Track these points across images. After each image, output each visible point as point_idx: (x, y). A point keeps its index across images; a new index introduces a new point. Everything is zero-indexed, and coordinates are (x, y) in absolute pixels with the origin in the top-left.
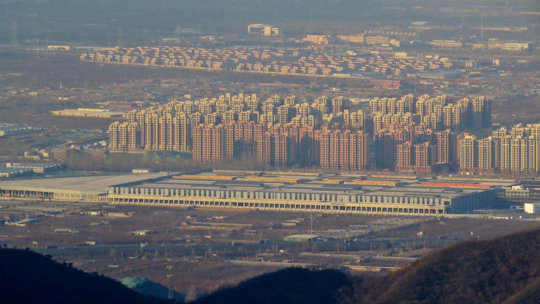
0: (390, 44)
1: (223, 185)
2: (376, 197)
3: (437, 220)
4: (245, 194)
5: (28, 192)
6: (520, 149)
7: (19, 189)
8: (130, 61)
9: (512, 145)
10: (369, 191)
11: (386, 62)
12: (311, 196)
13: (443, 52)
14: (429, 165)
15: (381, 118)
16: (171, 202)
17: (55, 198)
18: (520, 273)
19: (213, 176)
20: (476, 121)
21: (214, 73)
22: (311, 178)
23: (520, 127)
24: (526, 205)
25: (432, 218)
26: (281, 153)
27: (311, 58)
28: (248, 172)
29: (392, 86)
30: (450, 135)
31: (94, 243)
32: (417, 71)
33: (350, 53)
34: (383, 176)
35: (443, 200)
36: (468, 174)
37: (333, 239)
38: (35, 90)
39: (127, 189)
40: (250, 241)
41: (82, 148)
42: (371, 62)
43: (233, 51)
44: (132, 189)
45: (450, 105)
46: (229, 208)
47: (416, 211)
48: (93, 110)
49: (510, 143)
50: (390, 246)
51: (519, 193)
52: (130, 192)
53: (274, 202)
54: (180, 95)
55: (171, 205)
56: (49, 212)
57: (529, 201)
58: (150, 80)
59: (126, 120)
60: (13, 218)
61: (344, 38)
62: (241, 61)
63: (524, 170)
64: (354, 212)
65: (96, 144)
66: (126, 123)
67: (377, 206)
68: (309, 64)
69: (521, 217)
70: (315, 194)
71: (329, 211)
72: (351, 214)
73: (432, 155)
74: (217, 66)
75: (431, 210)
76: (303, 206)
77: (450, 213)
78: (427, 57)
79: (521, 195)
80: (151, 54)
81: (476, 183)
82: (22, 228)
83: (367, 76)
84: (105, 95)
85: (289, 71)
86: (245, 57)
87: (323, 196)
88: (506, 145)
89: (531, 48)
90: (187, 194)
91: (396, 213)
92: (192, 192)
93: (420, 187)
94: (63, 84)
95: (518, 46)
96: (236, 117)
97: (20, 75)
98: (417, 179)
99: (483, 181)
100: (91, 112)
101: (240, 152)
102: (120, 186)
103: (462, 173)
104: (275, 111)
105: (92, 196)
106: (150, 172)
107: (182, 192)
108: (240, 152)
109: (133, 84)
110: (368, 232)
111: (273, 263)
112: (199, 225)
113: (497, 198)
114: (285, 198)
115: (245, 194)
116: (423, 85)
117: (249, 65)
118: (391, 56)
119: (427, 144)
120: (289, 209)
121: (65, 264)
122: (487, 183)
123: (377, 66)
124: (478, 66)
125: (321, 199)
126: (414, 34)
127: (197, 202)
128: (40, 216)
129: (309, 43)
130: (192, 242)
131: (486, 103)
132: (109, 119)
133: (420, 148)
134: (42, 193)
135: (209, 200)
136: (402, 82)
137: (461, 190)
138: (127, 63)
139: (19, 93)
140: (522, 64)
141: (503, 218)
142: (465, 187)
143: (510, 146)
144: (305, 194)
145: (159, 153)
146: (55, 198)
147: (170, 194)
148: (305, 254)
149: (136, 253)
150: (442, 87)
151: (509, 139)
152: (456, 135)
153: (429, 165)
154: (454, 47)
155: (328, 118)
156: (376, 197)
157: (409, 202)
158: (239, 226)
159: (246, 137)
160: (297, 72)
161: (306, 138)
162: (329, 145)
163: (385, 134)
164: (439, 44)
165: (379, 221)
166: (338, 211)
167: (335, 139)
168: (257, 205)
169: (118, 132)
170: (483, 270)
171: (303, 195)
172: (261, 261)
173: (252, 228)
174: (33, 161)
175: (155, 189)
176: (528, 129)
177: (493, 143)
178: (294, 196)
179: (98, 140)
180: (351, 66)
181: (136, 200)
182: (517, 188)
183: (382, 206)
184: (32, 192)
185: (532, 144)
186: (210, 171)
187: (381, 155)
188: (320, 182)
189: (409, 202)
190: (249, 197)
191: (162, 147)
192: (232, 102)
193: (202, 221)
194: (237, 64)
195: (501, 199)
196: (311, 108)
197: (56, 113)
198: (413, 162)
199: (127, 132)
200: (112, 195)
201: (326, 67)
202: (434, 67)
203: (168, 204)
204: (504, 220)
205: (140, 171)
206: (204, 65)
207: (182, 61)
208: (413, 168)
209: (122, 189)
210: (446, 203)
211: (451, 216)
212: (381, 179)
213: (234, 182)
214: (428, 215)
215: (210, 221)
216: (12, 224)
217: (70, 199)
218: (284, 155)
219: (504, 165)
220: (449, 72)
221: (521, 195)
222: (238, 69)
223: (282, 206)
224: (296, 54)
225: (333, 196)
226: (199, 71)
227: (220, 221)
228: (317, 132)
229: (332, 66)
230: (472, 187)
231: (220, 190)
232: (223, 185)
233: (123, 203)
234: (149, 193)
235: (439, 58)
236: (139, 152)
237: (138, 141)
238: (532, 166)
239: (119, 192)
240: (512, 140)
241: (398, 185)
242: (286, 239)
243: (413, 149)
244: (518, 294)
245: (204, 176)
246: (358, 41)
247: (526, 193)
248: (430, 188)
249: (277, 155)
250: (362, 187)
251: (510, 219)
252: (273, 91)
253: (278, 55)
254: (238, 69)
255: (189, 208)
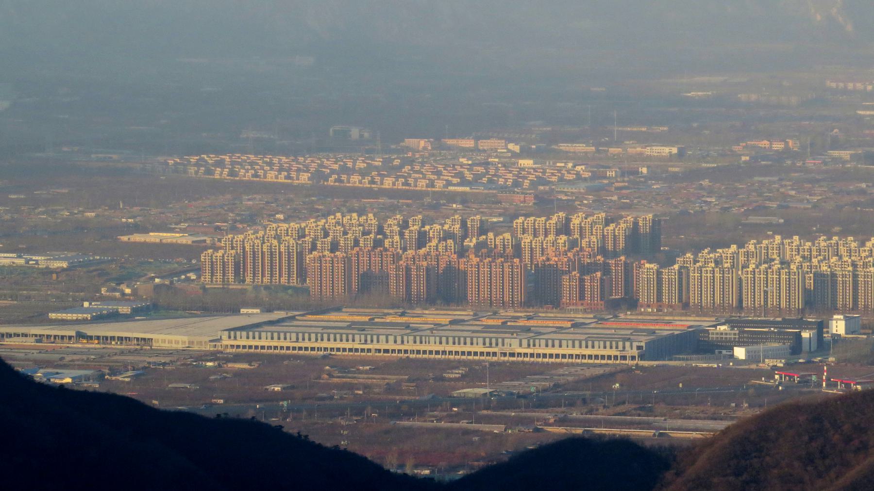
0: (507, 149)
1: (361, 327)
2: (553, 340)
4: (391, 338)
5: (121, 339)
7: (109, 334)
8: (197, 172)
9: (704, 275)
10: (540, 334)
11: (511, 172)
12: (472, 340)
13: (578, 159)
15: (531, 242)
16: (300, 349)
17: (155, 345)
18: (856, 443)
19: (344, 317)
20: (639, 244)
21: (302, 187)
22: (466, 318)
23: (709, 253)
24: (736, 349)
26: (419, 286)
27: (417, 168)
28: (386, 311)
29: (525, 202)
30: (625, 263)
31: (222, 401)
32: (550, 182)
33: (463, 160)
34: (552, 315)
35: (635, 344)
37: (512, 394)
38: (92, 209)
39: (244, 334)
40: (411, 398)
41: (172, 283)
42: (492, 172)
43: (319, 159)
44: (251, 334)
45: (612, 226)
46: (372, 356)
47: (603, 357)
48: (169, 235)
50: (584, 401)
51: (726, 334)
52: (248, 338)
53: (427, 348)
54: (270, 216)
55: (301, 352)
56: (155, 363)
57: (740, 344)
58: (229, 196)
59: (221, 248)
60: (114, 372)
61: (450, 142)
62: (333, 172)
63: (719, 305)
64: (527, 359)
65: (183, 277)
66: (222, 251)
67: (555, 351)
68: (417, 175)
70: (477, 338)
71: (495, 359)
72: (523, 362)
73: (605, 287)
74: (304, 178)
76: (463, 353)
78: (558, 164)
80: (220, 164)
81: (669, 323)
82: (128, 383)
83: (490, 189)
84: (178, 215)
85: (394, 184)
86: (336, 167)
87: (487, 340)
89: (681, 154)
90: (319, 339)
91: (579, 361)
92: (325, 336)
94: (123, 202)
95: (666, 150)
96: (356, 242)
97: (67, 191)
98: (594, 317)
100: (167, 237)
101: (367, 286)
102: (235, 329)
104: (402, 234)
105: (201, 342)
106: (262, 311)
107: (313, 336)
108: (367, 286)
109: (208, 202)
110: (552, 384)
111: (449, 425)
112: (343, 377)
114: (441, 343)
115: (391, 338)
116: (561, 200)
117: (344, 177)
118: (514, 164)
119: (599, 274)
120: (440, 356)
121: (300, 436)
122: (682, 323)
123: (500, 177)
124: (623, 175)
125: (484, 344)
126: (534, 136)
127: (332, 349)
128: (145, 368)
129: (408, 149)
130: (342, 398)
131: (656, 223)
132: (190, 245)
134: (138, 339)
135: (348, 346)
136: (536, 197)
137: (653, 332)
138: (194, 175)
139: (72, 214)
140: (675, 173)
142: (657, 327)
143: (754, 278)
144: (465, 338)
145: (267, 288)
146: (155, 345)
147: (298, 338)
148: (485, 412)
149: (279, 414)
150: (585, 202)
151: (701, 267)
152: (632, 264)
153: (601, 300)
154: (586, 153)
155: (471, 242)
156: (553, 340)
157: (593, 347)
158: (393, 379)
159: (373, 268)
160: (403, 184)
161: (449, 268)
162: (478, 277)
163: (547, 263)
164: (567, 149)
165: (561, 371)
166: (506, 359)
167: (486, 269)
168: (406, 351)
169: (212, 262)
170: (811, 439)
171: (462, 340)
172: (433, 421)
173: (409, 381)
174: (114, 299)
175: (279, 333)
177: (680, 273)
178: (451, 340)
179: (185, 272)
180: (469, 176)
181: (256, 347)
182: (723, 328)
183: (561, 351)
184: (126, 338)
186: (338, 309)
187: (542, 289)
188: (478, 323)
190: (395, 342)
191: (266, 280)
192: (350, 224)
193: (345, 372)
194: (330, 175)
196: (445, 231)
197: (125, 238)
198: (582, 297)
199: (224, 262)
200: (226, 342)
201: (439, 179)
202: (571, 177)
203: (295, 352)
205: (250, 311)
206: (288, 177)
207: (261, 173)
208: (582, 304)
209: (238, 333)
210: (639, 348)
211: (646, 363)
212: (547, 319)
213: (371, 322)
214: (618, 362)
215: (354, 372)
216: (114, 378)
217: (174, 346)
218: (423, 289)
219: (694, 299)
220: (588, 184)
222: (331, 181)
223: (437, 352)
224: (397, 162)
225: (500, 340)
226: (283, 185)
227: (366, 372)
228: (462, 260)
229: (446, 178)
230: (666, 328)
231: (360, 335)
232: (361, 327)
233: (240, 350)
234: (272, 338)
235: (574, 166)
236: (240, 287)
237: (237, 272)
239: (235, 338)
241: (573, 326)
242: (455, 393)
243: (582, 281)
244: (858, 468)
245: (333, 316)
246: (467, 146)
247: (735, 334)
248: (615, 329)
249: (414, 287)
252: (382, 208)
253: (376, 163)
254: (331, 181)
255: (324, 357)
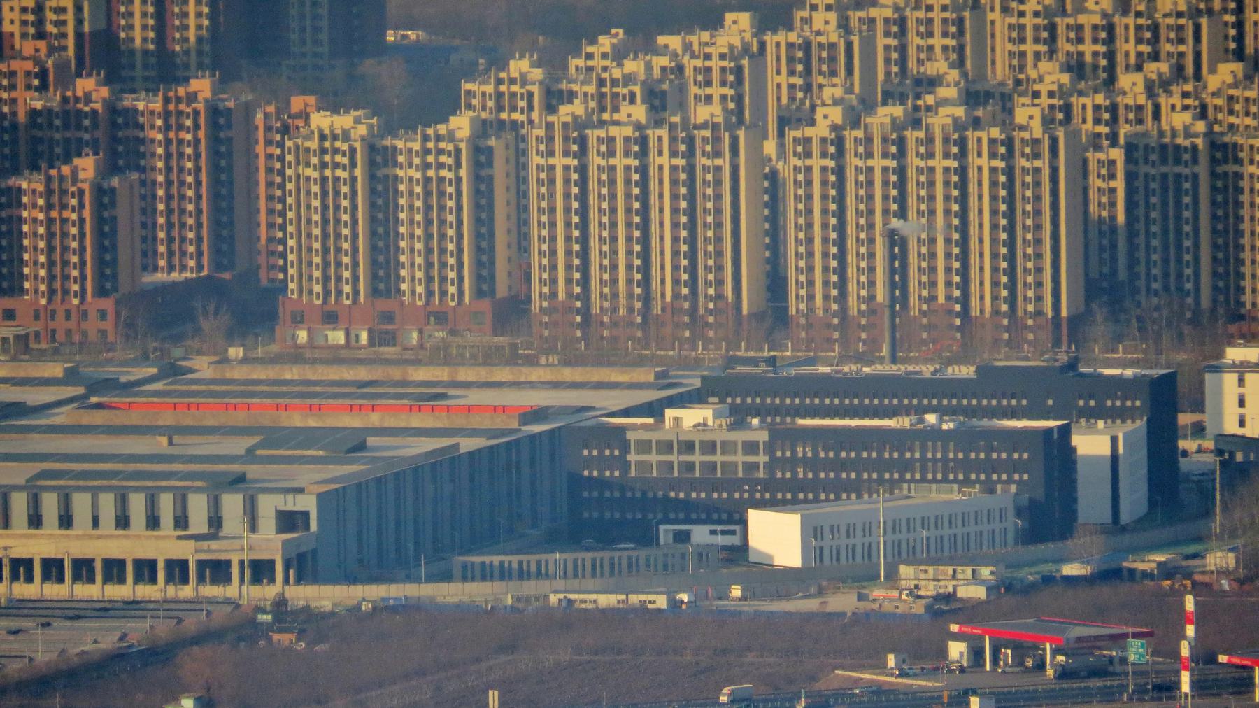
3: (253, 622)
6: (644, 183)
9: (595, 160)
14: (101, 292)
22: (34, 396)
23: (619, 55)
24: (754, 516)
25: (221, 615)
30: (215, 112)
36: (337, 337)
47: (114, 570)
49: (583, 152)
51: (710, 447)
69: (736, 591)
75: (201, 564)
77: (316, 579)
79: (718, 458)
81: (431, 397)
88: (558, 161)
93: (110, 430)
98: (71, 377)
99: (467, 385)
103: (303, 336)
113: (576, 482)
119: (87, 166)
122: (501, 397)
133: (49, 192)
137: (356, 445)
141: (635, 599)
142: (375, 419)
143: (583, 170)
152: (248, 110)
153: (101, 292)
176: (664, 61)
177: (481, 156)
182: (691, 417)
185: (717, 154)
189: (66, 521)
195: (601, 483)
204: (642, 609)
210: (289, 521)
211: (322, 597)
214: (187, 591)
219: (549, 283)
221: (718, 458)
238: (720, 282)
240: (593, 134)
247: (751, 448)
248: (171, 432)
250: (371, 441)
251: (675, 604)
